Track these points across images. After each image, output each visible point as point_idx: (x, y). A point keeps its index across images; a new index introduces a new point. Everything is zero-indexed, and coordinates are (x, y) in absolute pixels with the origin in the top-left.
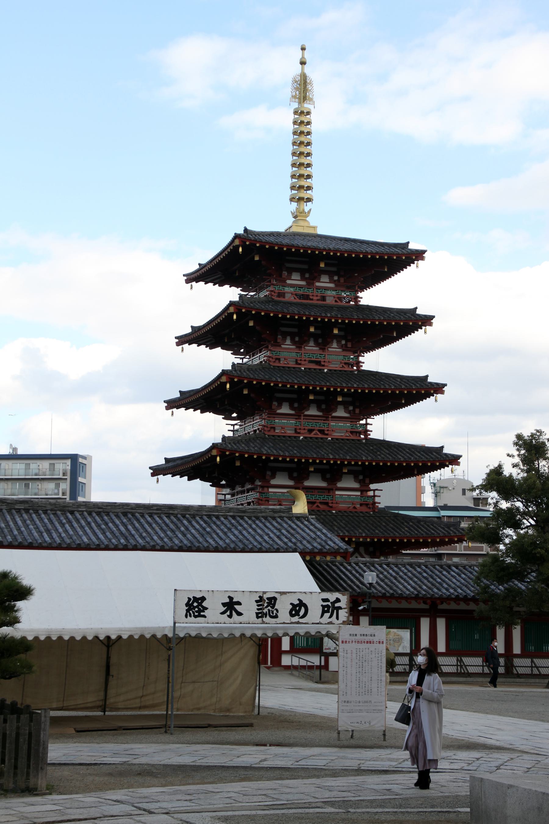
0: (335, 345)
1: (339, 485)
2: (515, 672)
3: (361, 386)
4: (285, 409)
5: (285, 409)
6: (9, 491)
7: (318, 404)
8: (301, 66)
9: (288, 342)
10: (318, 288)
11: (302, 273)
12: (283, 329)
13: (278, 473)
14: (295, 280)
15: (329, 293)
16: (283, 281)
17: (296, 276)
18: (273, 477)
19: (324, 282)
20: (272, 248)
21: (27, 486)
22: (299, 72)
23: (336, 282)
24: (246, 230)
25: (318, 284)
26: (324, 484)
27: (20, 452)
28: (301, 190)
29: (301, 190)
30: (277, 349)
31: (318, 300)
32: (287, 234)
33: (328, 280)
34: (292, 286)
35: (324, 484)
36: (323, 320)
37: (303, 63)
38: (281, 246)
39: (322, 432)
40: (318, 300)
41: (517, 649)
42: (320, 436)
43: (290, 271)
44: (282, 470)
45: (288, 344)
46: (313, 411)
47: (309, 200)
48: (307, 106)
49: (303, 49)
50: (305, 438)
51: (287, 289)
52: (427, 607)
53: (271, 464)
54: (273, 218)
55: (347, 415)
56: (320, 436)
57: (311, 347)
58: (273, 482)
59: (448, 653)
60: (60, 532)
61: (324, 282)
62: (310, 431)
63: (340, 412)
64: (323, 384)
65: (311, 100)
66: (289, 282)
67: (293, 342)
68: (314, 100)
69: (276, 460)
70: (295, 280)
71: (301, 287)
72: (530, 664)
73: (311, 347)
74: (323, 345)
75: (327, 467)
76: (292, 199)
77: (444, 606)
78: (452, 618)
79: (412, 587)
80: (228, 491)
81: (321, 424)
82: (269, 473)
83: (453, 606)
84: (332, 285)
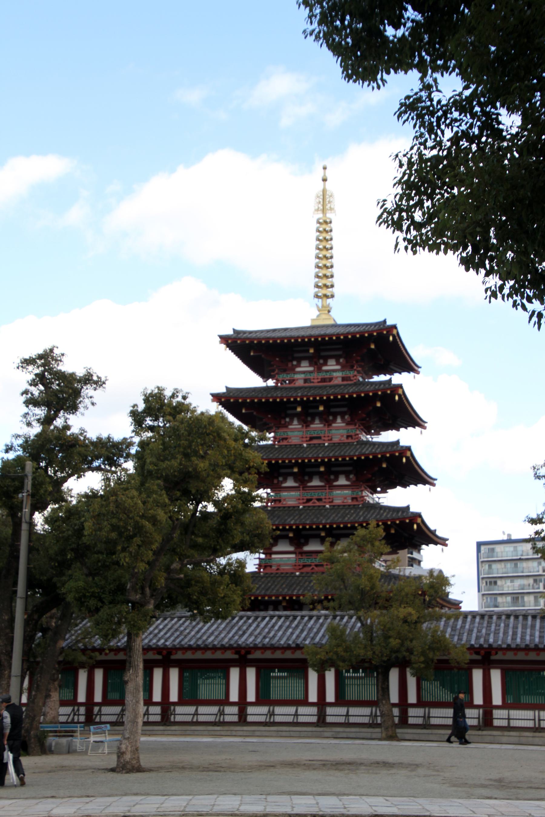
0: (339, 420)
2: (172, 720)
3: (326, 455)
4: (290, 483)
5: (290, 483)
6: (500, 571)
7: (321, 476)
8: (322, 182)
13: (342, 539)
14: (305, 367)
15: (335, 374)
16: (292, 370)
20: (260, 342)
21: (516, 565)
22: (321, 188)
27: (513, 537)
28: (324, 287)
29: (324, 287)
30: (285, 430)
31: (318, 382)
32: (312, 327)
33: (307, 364)
37: (325, 180)
38: (275, 340)
39: (319, 500)
40: (318, 382)
41: (497, 699)
42: (318, 504)
43: (299, 360)
45: (296, 424)
46: (316, 482)
47: (333, 296)
48: (329, 215)
49: (325, 168)
50: (304, 507)
51: (296, 376)
53: (304, 533)
54: (294, 314)
56: (318, 504)
57: (317, 425)
58: (275, 549)
59: (259, 702)
61: (332, 365)
62: (308, 500)
63: (342, 481)
64: (290, 456)
65: (331, 209)
66: (298, 369)
68: (336, 209)
69: (338, 528)
70: (305, 367)
71: (310, 372)
72: (511, 721)
73: (317, 425)
74: (328, 423)
76: (317, 296)
77: (499, 656)
78: (184, 666)
81: (322, 494)
84: (338, 367)
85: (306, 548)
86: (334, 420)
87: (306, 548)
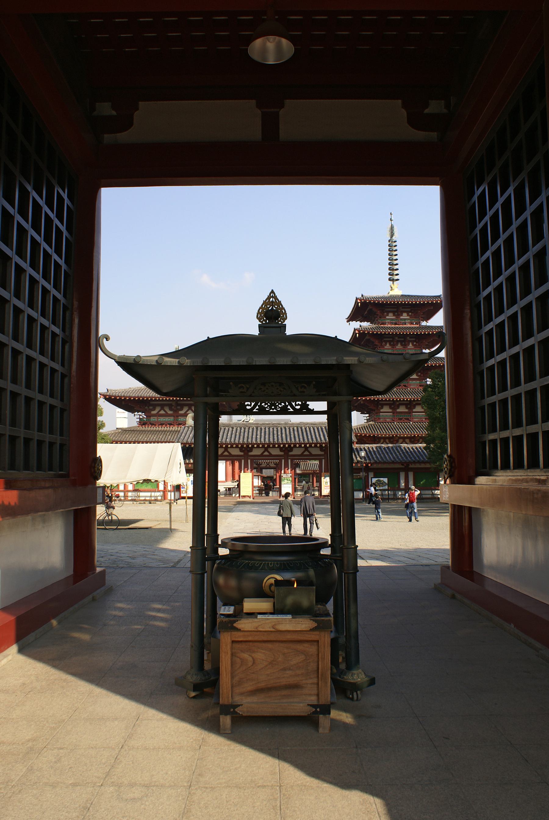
1: (414, 410)
9: (388, 345)
10: (402, 319)
11: (394, 313)
12: (385, 339)
14: (391, 316)
15: (407, 321)
17: (391, 314)
18: (382, 408)
19: (405, 316)
23: (411, 316)
24: (362, 296)
25: (401, 317)
26: (407, 411)
34: (388, 319)
35: (407, 411)
36: (403, 333)
37: (391, 220)
43: (388, 312)
44: (386, 404)
49: (391, 214)
52: (403, 467)
54: (380, 289)
55: (417, 377)
60: (154, 438)
61: (405, 316)
66: (387, 317)
67: (390, 345)
70: (391, 316)
73: (399, 346)
75: (392, 402)
78: (416, 472)
79: (381, 457)
80: (368, 415)
82: (380, 406)
83: (418, 466)
84: (408, 317)
85: (398, 410)
86: (397, 345)
87: (398, 410)
